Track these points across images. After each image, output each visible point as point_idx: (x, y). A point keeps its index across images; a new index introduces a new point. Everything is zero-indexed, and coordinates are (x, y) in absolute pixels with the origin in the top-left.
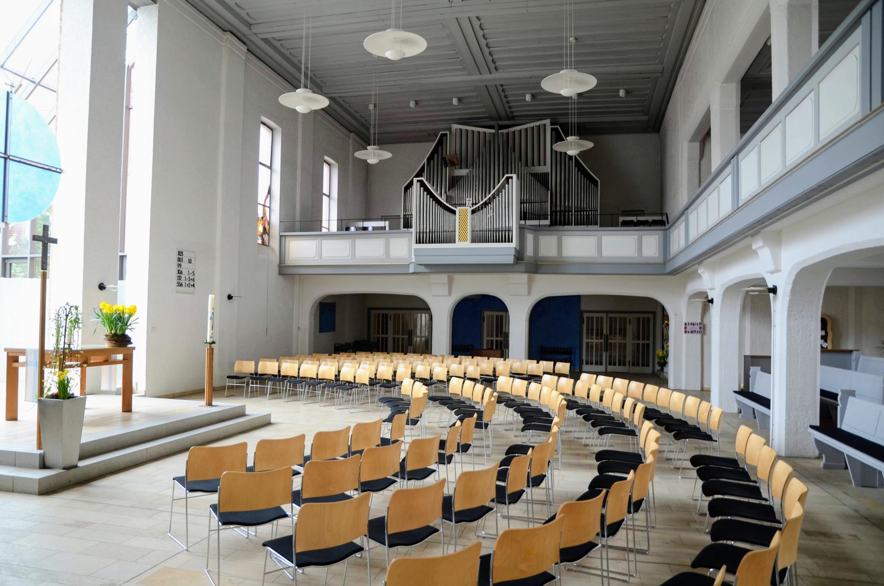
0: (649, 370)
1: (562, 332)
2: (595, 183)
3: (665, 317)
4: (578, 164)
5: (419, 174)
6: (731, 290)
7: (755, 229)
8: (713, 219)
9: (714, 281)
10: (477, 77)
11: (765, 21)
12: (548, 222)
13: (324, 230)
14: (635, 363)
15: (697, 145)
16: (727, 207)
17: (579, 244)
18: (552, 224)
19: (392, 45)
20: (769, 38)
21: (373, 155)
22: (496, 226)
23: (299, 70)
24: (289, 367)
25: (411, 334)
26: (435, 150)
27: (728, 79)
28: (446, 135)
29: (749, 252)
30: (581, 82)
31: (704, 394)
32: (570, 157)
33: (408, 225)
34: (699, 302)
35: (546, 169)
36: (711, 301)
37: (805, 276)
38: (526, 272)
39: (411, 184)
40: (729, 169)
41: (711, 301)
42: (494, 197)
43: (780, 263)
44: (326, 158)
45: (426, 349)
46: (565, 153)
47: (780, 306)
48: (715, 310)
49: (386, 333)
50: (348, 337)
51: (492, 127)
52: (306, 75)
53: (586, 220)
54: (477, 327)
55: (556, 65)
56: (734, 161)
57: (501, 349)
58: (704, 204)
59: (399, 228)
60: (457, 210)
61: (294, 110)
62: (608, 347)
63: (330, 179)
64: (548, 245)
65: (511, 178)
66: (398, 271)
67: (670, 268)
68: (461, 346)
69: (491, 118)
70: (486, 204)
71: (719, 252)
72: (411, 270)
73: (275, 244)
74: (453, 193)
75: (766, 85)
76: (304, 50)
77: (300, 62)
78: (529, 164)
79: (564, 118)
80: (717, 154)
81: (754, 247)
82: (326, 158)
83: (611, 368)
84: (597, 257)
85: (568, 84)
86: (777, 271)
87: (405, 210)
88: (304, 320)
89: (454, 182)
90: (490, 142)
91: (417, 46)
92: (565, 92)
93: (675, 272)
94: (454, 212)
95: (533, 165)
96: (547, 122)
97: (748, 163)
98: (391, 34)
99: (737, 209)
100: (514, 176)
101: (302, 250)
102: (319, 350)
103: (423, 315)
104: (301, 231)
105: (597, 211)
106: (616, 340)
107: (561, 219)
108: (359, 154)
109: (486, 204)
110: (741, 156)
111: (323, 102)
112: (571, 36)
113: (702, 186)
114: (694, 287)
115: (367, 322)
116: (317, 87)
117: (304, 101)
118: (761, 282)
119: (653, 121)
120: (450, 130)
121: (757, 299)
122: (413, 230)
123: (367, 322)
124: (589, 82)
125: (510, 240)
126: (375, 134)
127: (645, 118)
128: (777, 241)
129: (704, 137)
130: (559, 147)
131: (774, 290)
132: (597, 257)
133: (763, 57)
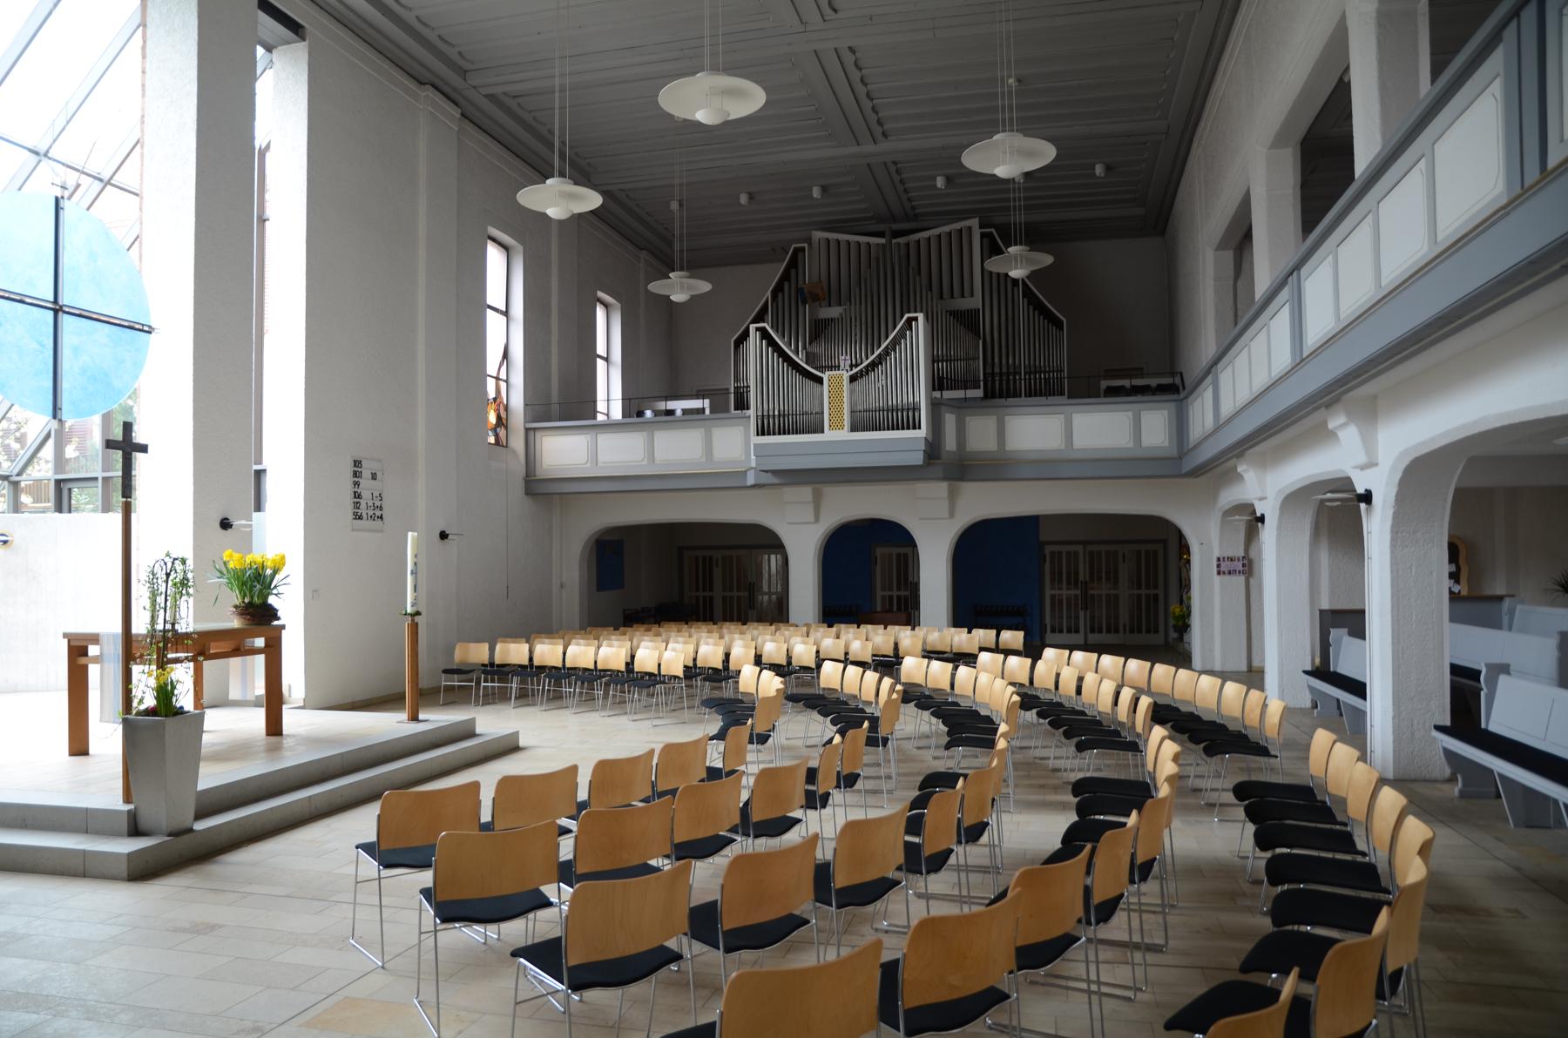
0: (1158, 639)
2: (1058, 324)
3: (1184, 548)
5: (759, 318)
6: (1293, 499)
7: (1332, 395)
8: (1261, 380)
9: (1266, 485)
10: (854, 149)
11: (1338, 42)
12: (979, 393)
13: (600, 417)
14: (1135, 629)
15: (1229, 255)
16: (1283, 358)
17: (1034, 430)
18: (986, 397)
19: (708, 100)
20: (1347, 69)
21: (679, 288)
23: (551, 146)
24: (548, 652)
25: (753, 589)
26: (785, 277)
27: (1279, 141)
29: (1323, 435)
30: (1030, 154)
32: (1015, 282)
33: (742, 404)
34: (1241, 520)
35: (974, 302)
38: (945, 479)
40: (1285, 294)
41: (1262, 519)
42: (887, 352)
43: (1371, 454)
44: (600, 294)
45: (777, 614)
47: (1377, 526)
48: (1268, 534)
49: (711, 590)
51: (880, 234)
52: (562, 155)
54: (866, 575)
55: (986, 126)
57: (906, 611)
59: (727, 410)
60: (825, 376)
63: (608, 333)
64: (981, 433)
66: (727, 483)
67: (1186, 468)
72: (751, 481)
73: (517, 443)
74: (819, 349)
77: (552, 133)
79: (1002, 214)
80: (1263, 279)
81: (1331, 425)
82: (600, 294)
84: (1069, 448)
85: (1006, 158)
86: (1371, 464)
87: (737, 379)
89: (820, 330)
91: (749, 100)
92: (1002, 171)
94: (820, 381)
96: (974, 222)
97: (1316, 283)
98: (705, 81)
101: (564, 451)
103: (773, 557)
107: (1004, 387)
108: (656, 287)
109: (873, 365)
111: (592, 200)
113: (1241, 325)
114: (1231, 496)
116: (582, 175)
117: (558, 199)
118: (1345, 484)
120: (809, 240)
121: (1337, 513)
122: (751, 412)
123: (678, 570)
125: (916, 426)
126: (681, 251)
128: (1369, 414)
129: (1240, 239)
130: (995, 265)
131: (1367, 497)
132: (1069, 448)
133: (1338, 102)
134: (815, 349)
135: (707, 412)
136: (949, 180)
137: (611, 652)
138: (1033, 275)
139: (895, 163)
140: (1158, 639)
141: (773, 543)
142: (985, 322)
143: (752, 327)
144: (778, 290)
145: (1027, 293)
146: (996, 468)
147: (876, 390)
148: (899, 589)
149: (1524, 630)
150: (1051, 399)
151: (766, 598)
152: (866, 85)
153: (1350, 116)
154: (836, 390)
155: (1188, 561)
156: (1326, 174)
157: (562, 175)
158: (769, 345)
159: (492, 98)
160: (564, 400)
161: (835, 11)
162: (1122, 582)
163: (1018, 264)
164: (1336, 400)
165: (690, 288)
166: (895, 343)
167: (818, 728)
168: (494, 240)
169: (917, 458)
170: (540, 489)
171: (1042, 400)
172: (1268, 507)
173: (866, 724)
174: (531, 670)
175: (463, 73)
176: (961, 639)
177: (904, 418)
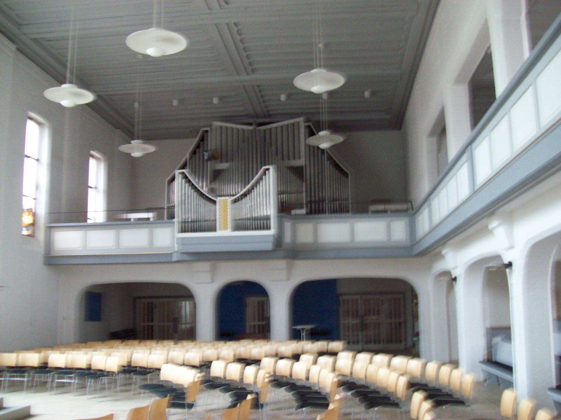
0: (402, 346)
1: (322, 312)
2: (345, 174)
3: (414, 296)
4: (330, 158)
5: (184, 167)
6: (474, 266)
7: (491, 210)
8: (453, 203)
9: (457, 260)
10: (237, 78)
11: (484, 34)
12: (303, 211)
13: (89, 222)
14: (390, 341)
15: (434, 140)
16: (465, 192)
17: (334, 231)
18: (307, 214)
19: (155, 43)
20: (489, 48)
21: (137, 149)
22: (255, 215)
23: (65, 66)
24: (58, 359)
25: (176, 320)
26: (198, 146)
27: (458, 81)
28: (207, 131)
29: (485, 232)
30: (330, 81)
31: (455, 364)
32: (323, 151)
33: (172, 216)
34: (446, 279)
35: (301, 162)
36: (455, 279)
37: (538, 249)
38: (285, 258)
39: (173, 179)
40: (465, 157)
41: (455, 279)
42: (252, 188)
43: (512, 240)
44: (93, 152)
45: (190, 335)
46: (318, 148)
47: (516, 280)
48: (460, 287)
49: (152, 321)
50: (116, 327)
51: (250, 124)
52: (72, 72)
53: (340, 209)
54: (241, 312)
55: (307, 66)
56: (469, 147)
57: (263, 332)
58: (453, 182)
59: (163, 219)
60: (218, 200)
61: (60, 104)
62: (364, 326)
63: (97, 172)
64: (305, 232)
65: (268, 169)
66: (162, 259)
67: (416, 252)
68: (227, 331)
69: (249, 116)
70: (245, 195)
71: (463, 231)
72: (175, 259)
73: (41, 235)
74: (216, 186)
75: (491, 87)
76: (70, 50)
77: (67, 61)
78: (286, 157)
79: (315, 114)
80: (453, 146)
81: (491, 227)
82: (93, 152)
83: (366, 346)
84: (353, 239)
85: (319, 82)
86: (511, 247)
87: (169, 202)
88: (70, 309)
89: (217, 175)
90: (248, 138)
91: (177, 44)
92: (316, 89)
93: (422, 254)
94: (214, 202)
95: (289, 159)
96: (301, 119)
97: (481, 150)
98: (154, 33)
99: (475, 193)
100: (272, 168)
101: (69, 241)
102: (85, 339)
103: (188, 303)
104: (65, 222)
105: (348, 200)
106: (372, 318)
107: (317, 209)
108: (124, 148)
109: (245, 195)
110: (474, 145)
111: (88, 97)
112: (320, 43)
113: (441, 176)
114: (440, 266)
115: (133, 310)
116: (84, 83)
117: (69, 96)
118: (498, 257)
119: (396, 119)
120: (211, 126)
121: (496, 275)
122: (176, 220)
123: (133, 310)
124: (337, 81)
125: (268, 228)
126: (138, 130)
127: (389, 117)
128: (510, 219)
129: (440, 131)
130: (312, 141)
131: (510, 265)
132: (353, 239)
133: (486, 65)
134: (213, 186)
135: (151, 220)
136: (289, 96)
137: (80, 358)
138: (334, 147)
139: (236, 24)
140: (402, 346)
141: (188, 295)
142: (308, 172)
143: (177, 172)
144: (194, 152)
145: (330, 158)
146: (313, 252)
147: (248, 209)
148: (259, 320)
149: (458, 356)
150: (343, 215)
151: (184, 326)
152: (240, 35)
153: (492, 70)
154: (224, 209)
155: (417, 304)
156: (483, 98)
157: (71, 82)
158: (186, 182)
159: (35, 40)
160: (69, 209)
161: (227, 3)
162: (379, 313)
163: (325, 140)
164: (492, 214)
165: (143, 149)
166: (258, 182)
167: (223, 399)
168: (31, 119)
169: (269, 246)
170: (54, 262)
171: (338, 215)
172: (459, 272)
173: (249, 397)
174: (20, 370)
175: (19, 25)
176: (291, 347)
177: (261, 223)
